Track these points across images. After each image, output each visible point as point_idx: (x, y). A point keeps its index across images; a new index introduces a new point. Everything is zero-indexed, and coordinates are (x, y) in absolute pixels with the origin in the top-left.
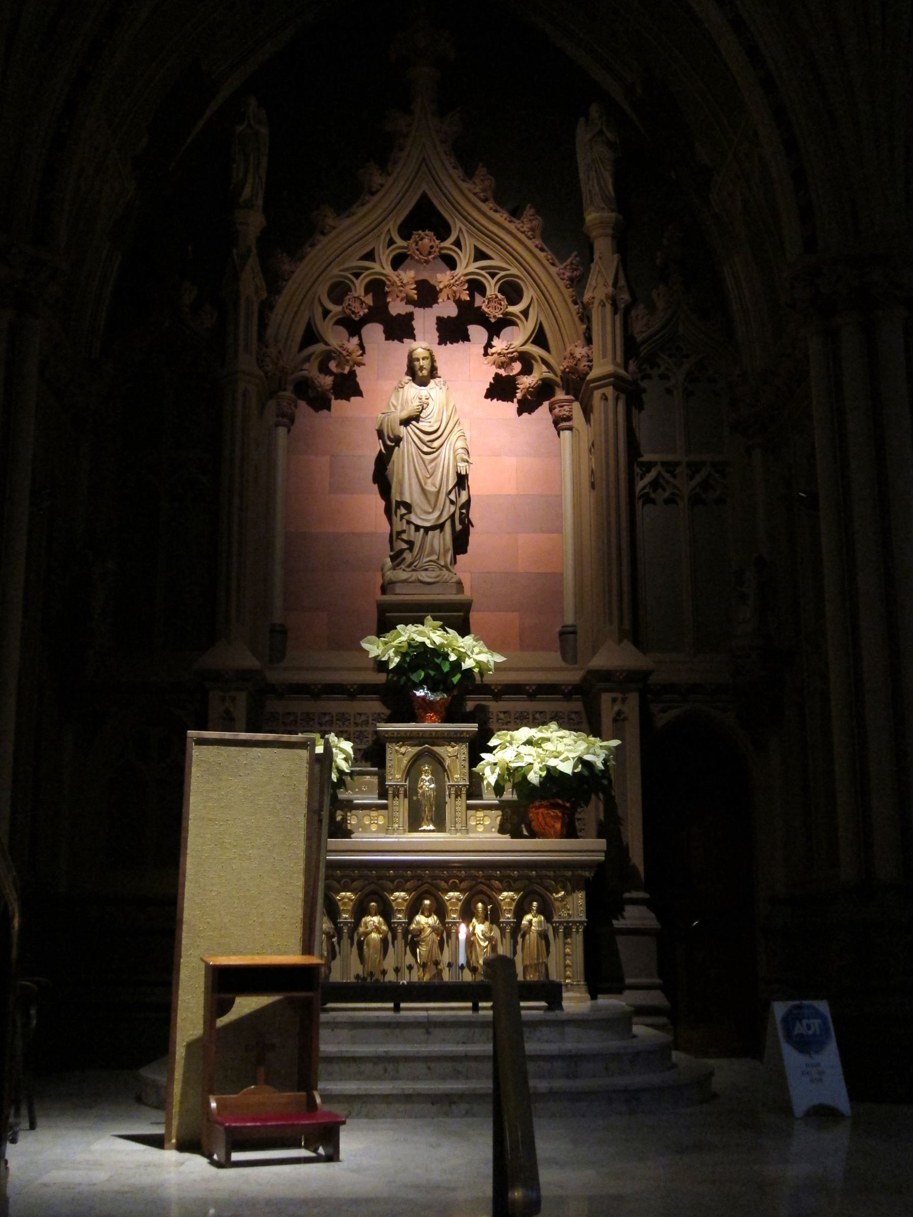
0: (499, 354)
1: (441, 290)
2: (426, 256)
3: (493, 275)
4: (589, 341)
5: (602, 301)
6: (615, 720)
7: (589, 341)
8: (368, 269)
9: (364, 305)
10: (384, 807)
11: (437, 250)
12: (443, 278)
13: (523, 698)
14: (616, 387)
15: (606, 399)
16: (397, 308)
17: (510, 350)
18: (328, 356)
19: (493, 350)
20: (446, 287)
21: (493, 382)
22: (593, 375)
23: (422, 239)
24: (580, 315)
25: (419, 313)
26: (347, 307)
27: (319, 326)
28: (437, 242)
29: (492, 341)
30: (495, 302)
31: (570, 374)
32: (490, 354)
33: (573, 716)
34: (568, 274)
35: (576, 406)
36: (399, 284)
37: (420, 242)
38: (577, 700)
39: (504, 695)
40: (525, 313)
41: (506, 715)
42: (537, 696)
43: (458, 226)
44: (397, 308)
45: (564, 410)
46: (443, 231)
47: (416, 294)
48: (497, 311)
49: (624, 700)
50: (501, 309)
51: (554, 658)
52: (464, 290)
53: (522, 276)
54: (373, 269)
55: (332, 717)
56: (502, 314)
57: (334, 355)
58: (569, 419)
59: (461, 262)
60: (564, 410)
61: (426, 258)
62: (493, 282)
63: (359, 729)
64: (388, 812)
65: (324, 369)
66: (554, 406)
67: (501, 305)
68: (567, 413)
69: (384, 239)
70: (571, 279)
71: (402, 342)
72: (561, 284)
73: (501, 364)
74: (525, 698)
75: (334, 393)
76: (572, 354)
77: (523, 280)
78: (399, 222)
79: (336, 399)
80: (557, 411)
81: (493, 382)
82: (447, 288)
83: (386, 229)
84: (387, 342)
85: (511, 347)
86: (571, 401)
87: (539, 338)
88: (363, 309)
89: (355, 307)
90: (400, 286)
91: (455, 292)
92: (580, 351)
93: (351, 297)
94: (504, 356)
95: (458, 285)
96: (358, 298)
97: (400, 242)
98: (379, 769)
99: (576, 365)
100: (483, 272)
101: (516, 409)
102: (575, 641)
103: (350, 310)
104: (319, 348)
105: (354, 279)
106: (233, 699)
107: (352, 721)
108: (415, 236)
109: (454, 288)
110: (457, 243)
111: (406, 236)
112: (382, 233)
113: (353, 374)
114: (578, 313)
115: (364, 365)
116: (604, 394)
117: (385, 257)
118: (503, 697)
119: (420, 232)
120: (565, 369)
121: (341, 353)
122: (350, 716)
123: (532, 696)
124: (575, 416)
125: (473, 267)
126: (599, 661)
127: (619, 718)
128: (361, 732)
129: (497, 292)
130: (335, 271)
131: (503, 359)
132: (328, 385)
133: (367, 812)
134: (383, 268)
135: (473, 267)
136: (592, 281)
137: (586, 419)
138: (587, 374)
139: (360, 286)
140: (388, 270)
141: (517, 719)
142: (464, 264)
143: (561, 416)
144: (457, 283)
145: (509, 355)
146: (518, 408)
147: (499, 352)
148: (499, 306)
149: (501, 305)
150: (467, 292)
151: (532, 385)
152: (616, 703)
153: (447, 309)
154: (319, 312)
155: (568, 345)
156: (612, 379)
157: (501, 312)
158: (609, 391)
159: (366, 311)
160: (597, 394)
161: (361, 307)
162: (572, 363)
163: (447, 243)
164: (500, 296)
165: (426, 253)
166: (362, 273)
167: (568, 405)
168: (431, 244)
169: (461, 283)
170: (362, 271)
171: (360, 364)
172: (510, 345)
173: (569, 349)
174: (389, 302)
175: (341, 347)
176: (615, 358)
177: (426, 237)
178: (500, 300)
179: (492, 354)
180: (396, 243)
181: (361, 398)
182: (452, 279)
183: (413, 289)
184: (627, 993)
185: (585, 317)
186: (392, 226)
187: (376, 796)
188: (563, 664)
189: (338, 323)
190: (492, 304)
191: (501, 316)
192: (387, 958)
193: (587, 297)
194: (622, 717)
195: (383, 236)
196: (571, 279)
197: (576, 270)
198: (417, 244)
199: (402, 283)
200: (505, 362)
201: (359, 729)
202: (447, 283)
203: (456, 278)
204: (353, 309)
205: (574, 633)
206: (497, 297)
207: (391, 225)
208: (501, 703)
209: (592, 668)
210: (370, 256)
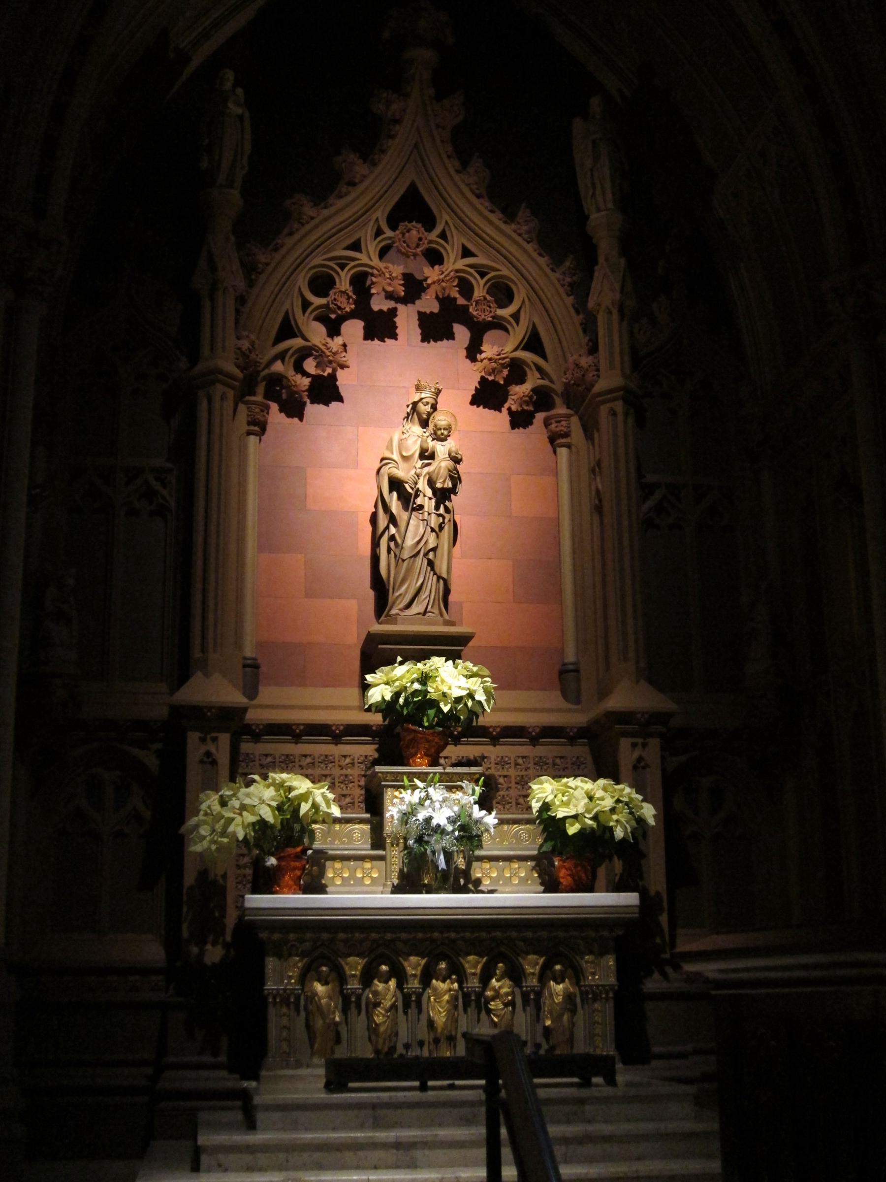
0: (490, 359)
1: (429, 286)
2: (415, 249)
3: (482, 275)
4: (593, 350)
5: (608, 308)
6: (635, 768)
7: (593, 350)
8: (353, 259)
9: (351, 300)
10: (382, 858)
11: (426, 242)
12: (432, 274)
13: (287, 739)
14: (626, 402)
15: (614, 414)
16: (379, 304)
17: (502, 356)
18: (305, 353)
19: (483, 355)
20: (434, 283)
21: (478, 387)
22: (597, 389)
23: (408, 231)
24: (583, 326)
25: (401, 308)
26: (332, 301)
27: (300, 322)
28: (426, 234)
29: (481, 346)
30: (484, 305)
31: (575, 386)
32: (479, 360)
33: (520, 761)
34: (568, 280)
35: (575, 420)
36: (387, 275)
37: (407, 234)
38: (584, 745)
39: (264, 735)
40: (516, 316)
41: (446, 760)
42: (343, 738)
43: (444, 218)
44: (379, 304)
45: (562, 426)
46: (429, 222)
47: (403, 291)
48: (487, 313)
49: (644, 745)
50: (491, 312)
51: (555, 699)
52: (455, 286)
53: (513, 277)
54: (361, 260)
55: (275, 758)
56: (491, 317)
57: (314, 353)
58: (567, 435)
59: (449, 258)
60: (562, 426)
61: (414, 251)
62: (482, 282)
63: (344, 772)
64: (386, 863)
65: (299, 368)
66: (550, 422)
67: (490, 307)
68: (565, 430)
69: (370, 230)
70: (571, 285)
71: (384, 341)
72: (561, 291)
73: (491, 371)
74: (289, 739)
75: (309, 397)
76: (577, 365)
77: (515, 284)
78: (389, 209)
79: (312, 402)
80: (553, 426)
81: (478, 387)
82: (436, 284)
83: (374, 218)
84: (366, 342)
85: (503, 352)
86: (568, 416)
87: (533, 343)
88: (350, 304)
89: (341, 302)
90: (388, 278)
91: (444, 289)
92: (585, 361)
93: (337, 290)
94: (495, 362)
95: (447, 281)
96: (344, 292)
97: (389, 233)
98: (371, 816)
99: (583, 376)
100: (472, 271)
101: (509, 423)
102: (578, 680)
103: (336, 305)
104: (297, 342)
105: (339, 270)
106: (215, 740)
107: (257, 763)
108: (402, 226)
109: (444, 284)
110: (443, 236)
111: (394, 228)
112: (370, 220)
113: (333, 377)
114: (581, 324)
115: (348, 367)
116: (612, 409)
117: (372, 247)
118: (541, 740)
119: (406, 223)
120: (569, 382)
121: (323, 352)
122: (255, 757)
123: (534, 741)
124: (573, 434)
125: (461, 264)
126: (617, 701)
127: (639, 766)
128: (346, 776)
129: (485, 294)
130: (318, 261)
131: (494, 365)
132: (305, 386)
133: (360, 863)
134: (371, 260)
135: (461, 264)
136: (595, 285)
137: (586, 436)
138: (593, 386)
139: (345, 279)
140: (376, 262)
141: (321, 763)
142: (452, 260)
143: (558, 432)
144: (448, 278)
145: (500, 361)
146: (510, 421)
147: (489, 357)
148: (488, 308)
149: (490, 307)
150: (457, 289)
151: (526, 393)
152: (636, 748)
153: (429, 304)
154: (298, 303)
155: (569, 355)
156: (621, 393)
157: (490, 315)
158: (619, 406)
159: (353, 306)
160: (604, 410)
161: (348, 302)
162: (578, 375)
163: (433, 235)
164: (489, 298)
165: (414, 245)
166: (348, 264)
167: (566, 421)
168: (419, 236)
169: (451, 278)
170: (348, 262)
171: (343, 367)
172: (502, 350)
173: (571, 360)
174: (373, 294)
175: (324, 345)
176: (622, 370)
177: (414, 229)
178: (489, 302)
179: (482, 361)
180: (384, 233)
181: (340, 404)
182: (441, 275)
183: (401, 285)
184: (655, 1063)
185: (589, 326)
186: (381, 214)
187: (369, 846)
188: (564, 705)
189: (317, 319)
190: (479, 307)
191: (491, 319)
192: (516, 1014)
193: (591, 304)
194: (642, 764)
195: (372, 223)
196: (571, 285)
197: (574, 275)
198: (403, 234)
199: (390, 275)
200: (495, 368)
201: (344, 772)
202: (436, 278)
203: (446, 273)
204: (339, 304)
205: (577, 671)
206: (485, 299)
207: (378, 214)
208: (340, 746)
209: (610, 709)
210: (356, 246)
